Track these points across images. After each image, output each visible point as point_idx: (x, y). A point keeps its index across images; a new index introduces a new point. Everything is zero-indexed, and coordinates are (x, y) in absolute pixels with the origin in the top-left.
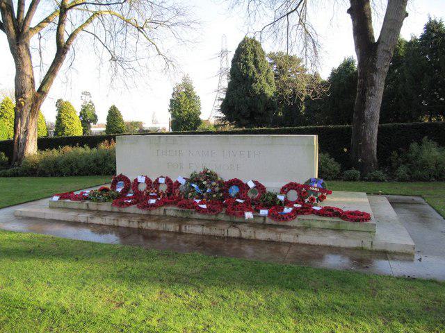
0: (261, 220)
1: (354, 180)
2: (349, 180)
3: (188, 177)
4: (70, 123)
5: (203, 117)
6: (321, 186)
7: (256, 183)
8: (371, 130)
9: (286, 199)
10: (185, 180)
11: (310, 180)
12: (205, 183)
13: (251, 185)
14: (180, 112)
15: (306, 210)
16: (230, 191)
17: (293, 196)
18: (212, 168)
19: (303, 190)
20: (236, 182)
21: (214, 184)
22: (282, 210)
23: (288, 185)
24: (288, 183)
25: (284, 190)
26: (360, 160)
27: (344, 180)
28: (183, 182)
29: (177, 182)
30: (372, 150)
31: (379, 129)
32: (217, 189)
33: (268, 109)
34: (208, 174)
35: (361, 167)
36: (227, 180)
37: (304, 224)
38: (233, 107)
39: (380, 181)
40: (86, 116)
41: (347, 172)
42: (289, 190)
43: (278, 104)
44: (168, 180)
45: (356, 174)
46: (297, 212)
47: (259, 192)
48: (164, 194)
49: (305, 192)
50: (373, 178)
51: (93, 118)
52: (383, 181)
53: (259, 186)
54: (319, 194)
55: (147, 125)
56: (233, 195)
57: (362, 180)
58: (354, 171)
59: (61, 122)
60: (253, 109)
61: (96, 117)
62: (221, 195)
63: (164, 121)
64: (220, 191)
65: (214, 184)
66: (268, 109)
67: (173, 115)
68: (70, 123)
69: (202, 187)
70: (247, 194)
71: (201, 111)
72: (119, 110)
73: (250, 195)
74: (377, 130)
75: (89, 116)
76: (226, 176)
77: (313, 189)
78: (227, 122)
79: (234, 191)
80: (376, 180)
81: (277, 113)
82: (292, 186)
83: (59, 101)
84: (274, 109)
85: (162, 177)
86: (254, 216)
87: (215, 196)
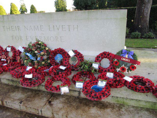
0: (76, 94)
1: (137, 38)
2: (135, 38)
3: (27, 46)
4: (16, 13)
5: (67, 8)
6: (131, 58)
7: (75, 52)
8: (147, 8)
9: (100, 67)
10: (23, 49)
11: (122, 51)
12: (36, 52)
13: (71, 54)
14: (59, 6)
15: (117, 82)
16: (56, 58)
17: (106, 63)
18: (42, 40)
19: (115, 60)
20: (61, 51)
21: (42, 53)
22: (97, 83)
23: (101, 54)
24: (102, 52)
25: (98, 59)
26: (140, 26)
27: (131, 38)
28: (22, 50)
29: (19, 50)
30: (146, 21)
31: (151, 8)
32: (45, 57)
33: (92, 4)
34: (40, 44)
35: (140, 30)
36: (53, 50)
37: (118, 101)
38: (79, 3)
39: (151, 38)
40: (22, 9)
41: (133, 33)
42: (102, 58)
43: (97, 2)
44: (13, 49)
45: (138, 35)
46: (111, 84)
47: (78, 60)
48: (11, 60)
49: (116, 62)
50: (147, 36)
51: (25, 10)
52: (153, 38)
53: (78, 55)
54: (129, 64)
55: (47, 11)
56: (58, 61)
57: (141, 38)
58: (137, 33)
59: (12, 12)
60: (86, 4)
61: (26, 9)
62: (49, 62)
63: (53, 9)
64: (49, 58)
65: (42, 53)
66: (92, 4)
67: (56, 8)
68: (16, 13)
69: (34, 55)
70: (68, 62)
71: (67, 6)
72: (35, 6)
73: (71, 62)
74: (150, 9)
75: (24, 9)
76: (53, 46)
77: (124, 59)
78: (77, 10)
79: (59, 58)
80: (150, 38)
81: (96, 6)
82: (105, 55)
83: (11, 3)
84: (95, 4)
85: (9, 46)
86: (70, 90)
87: (43, 63)
